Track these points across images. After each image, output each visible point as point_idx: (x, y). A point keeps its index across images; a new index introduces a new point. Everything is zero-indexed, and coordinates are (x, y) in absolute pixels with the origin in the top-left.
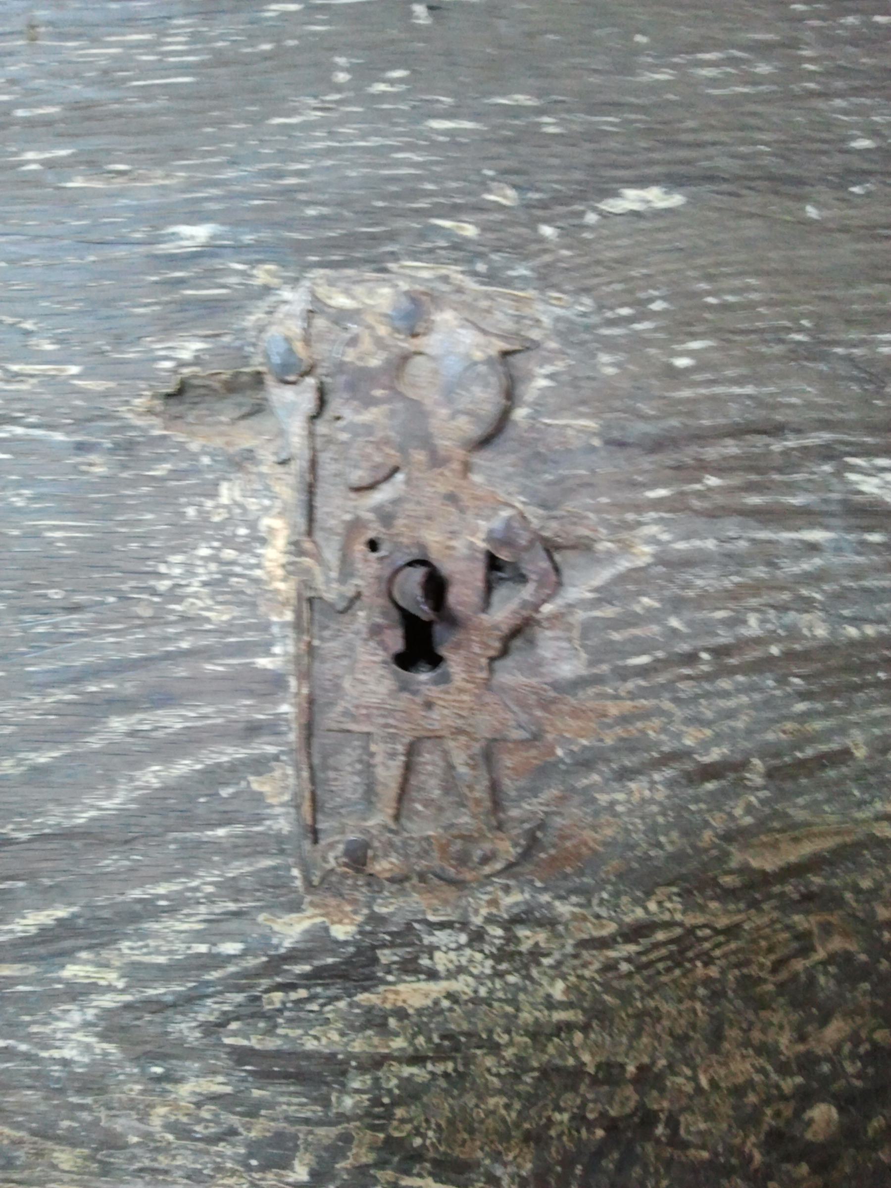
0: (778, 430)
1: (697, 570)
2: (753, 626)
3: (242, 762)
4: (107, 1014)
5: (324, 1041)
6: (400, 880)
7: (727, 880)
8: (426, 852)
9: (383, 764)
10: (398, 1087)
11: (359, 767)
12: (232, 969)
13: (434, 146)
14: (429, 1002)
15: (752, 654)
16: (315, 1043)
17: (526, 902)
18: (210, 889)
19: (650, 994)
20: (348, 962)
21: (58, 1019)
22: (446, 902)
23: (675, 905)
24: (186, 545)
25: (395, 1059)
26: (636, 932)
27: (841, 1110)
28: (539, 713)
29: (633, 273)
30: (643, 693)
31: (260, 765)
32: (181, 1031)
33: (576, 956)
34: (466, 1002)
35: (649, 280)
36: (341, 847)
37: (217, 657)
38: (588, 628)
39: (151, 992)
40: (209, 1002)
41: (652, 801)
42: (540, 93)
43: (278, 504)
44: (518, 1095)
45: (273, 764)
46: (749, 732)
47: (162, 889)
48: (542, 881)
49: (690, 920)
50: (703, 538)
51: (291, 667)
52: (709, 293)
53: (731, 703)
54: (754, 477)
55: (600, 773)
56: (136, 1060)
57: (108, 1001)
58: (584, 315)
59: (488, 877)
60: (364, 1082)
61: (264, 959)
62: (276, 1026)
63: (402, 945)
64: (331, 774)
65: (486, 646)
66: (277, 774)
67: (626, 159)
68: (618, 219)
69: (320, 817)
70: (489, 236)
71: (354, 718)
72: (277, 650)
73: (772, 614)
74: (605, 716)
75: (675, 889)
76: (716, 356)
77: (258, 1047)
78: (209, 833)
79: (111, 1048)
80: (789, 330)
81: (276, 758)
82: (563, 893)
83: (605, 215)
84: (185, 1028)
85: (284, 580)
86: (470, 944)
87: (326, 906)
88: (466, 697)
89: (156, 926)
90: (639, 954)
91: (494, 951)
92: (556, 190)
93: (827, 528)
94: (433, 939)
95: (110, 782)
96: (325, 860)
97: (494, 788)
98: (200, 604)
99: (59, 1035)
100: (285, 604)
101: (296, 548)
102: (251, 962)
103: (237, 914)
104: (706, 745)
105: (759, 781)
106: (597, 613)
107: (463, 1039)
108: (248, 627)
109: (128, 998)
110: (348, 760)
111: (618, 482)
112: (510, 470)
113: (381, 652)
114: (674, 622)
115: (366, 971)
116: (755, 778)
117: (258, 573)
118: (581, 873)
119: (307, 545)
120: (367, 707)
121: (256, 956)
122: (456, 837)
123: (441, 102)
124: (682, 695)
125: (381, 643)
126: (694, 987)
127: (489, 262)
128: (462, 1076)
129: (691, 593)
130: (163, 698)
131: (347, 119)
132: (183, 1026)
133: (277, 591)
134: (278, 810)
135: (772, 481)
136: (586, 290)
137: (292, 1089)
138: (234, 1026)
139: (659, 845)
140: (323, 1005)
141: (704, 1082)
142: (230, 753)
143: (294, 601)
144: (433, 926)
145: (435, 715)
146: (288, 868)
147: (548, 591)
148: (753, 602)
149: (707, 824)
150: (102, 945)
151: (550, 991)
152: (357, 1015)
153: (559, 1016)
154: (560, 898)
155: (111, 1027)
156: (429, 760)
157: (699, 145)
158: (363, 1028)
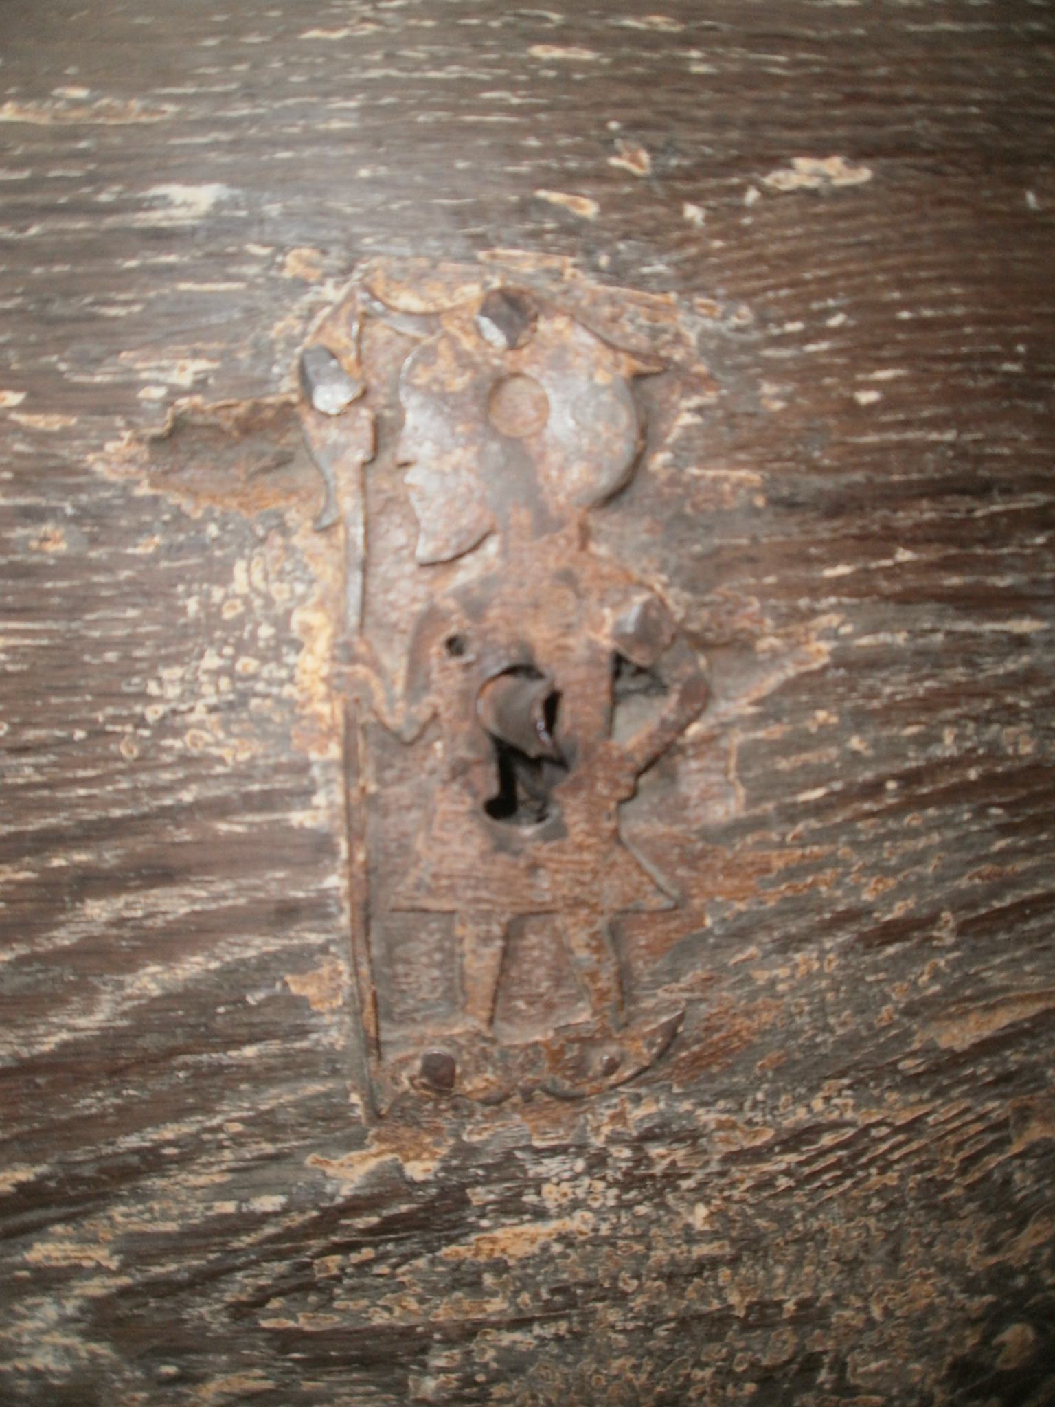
0: (983, 490)
1: (884, 674)
2: (948, 746)
3: (275, 956)
4: (97, 1305)
5: (397, 1311)
6: (496, 1102)
7: (906, 1065)
8: (533, 1063)
9: (474, 952)
10: (496, 1360)
11: (438, 957)
12: (270, 1230)
13: (535, 83)
14: (535, 1249)
15: (947, 781)
16: (386, 1315)
17: (661, 1113)
18: (238, 1127)
19: (813, 1213)
20: (429, 1207)
21: (23, 1317)
22: (557, 1122)
23: (848, 1099)
24: (188, 653)
27: (1040, 1330)
28: (682, 872)
29: (807, 276)
30: (816, 837)
31: (301, 960)
32: (201, 1318)
33: (722, 1174)
34: (583, 1244)
35: (826, 287)
36: (418, 1064)
38: (749, 754)
39: (156, 1270)
40: (239, 1276)
41: (820, 974)
42: (685, 15)
43: (317, 590)
44: (650, 1353)
45: (317, 957)
46: (940, 879)
47: (170, 1132)
48: (680, 1083)
49: (862, 1119)
51: (339, 823)
52: (903, 305)
53: (921, 843)
54: (953, 551)
55: (760, 944)
57: (95, 1287)
58: (739, 329)
60: (451, 1357)
61: (315, 1213)
62: (332, 1299)
65: (616, 784)
66: (325, 971)
68: (790, 198)
69: (384, 1025)
70: (616, 216)
71: (432, 892)
73: (971, 727)
74: (768, 871)
76: (907, 389)
77: (308, 1328)
78: (233, 1053)
79: (103, 1349)
80: (1000, 357)
81: (324, 949)
82: (707, 1098)
83: (766, 193)
84: (207, 1312)
85: (328, 698)
86: (588, 1171)
88: (587, 856)
90: (800, 1164)
91: (619, 1176)
93: (1036, 616)
94: (540, 1169)
95: (86, 991)
96: (396, 1081)
97: (624, 976)
98: (207, 737)
99: (26, 1339)
100: (330, 733)
101: (345, 653)
102: (297, 1219)
104: (887, 899)
105: (950, 940)
106: (760, 734)
107: (579, 1291)
108: (278, 769)
109: (125, 1281)
110: (423, 948)
111: (788, 556)
112: (645, 537)
114: (855, 743)
115: (453, 1217)
116: (945, 936)
117: (288, 690)
118: (730, 1070)
119: (361, 649)
120: (449, 877)
121: (302, 1211)
122: (572, 1041)
123: (547, 20)
124: (862, 838)
125: (467, 785)
126: (868, 1199)
127: (614, 254)
130: (162, 873)
131: (412, 37)
132: (204, 1310)
133: (318, 717)
134: (327, 1019)
136: (746, 296)
137: (355, 1376)
138: (275, 1304)
139: (827, 1028)
141: (876, 1312)
142: (257, 946)
143: (341, 730)
144: (540, 1153)
146: (346, 1094)
147: (697, 706)
148: (950, 713)
150: (86, 1214)
151: (690, 1220)
152: (440, 1274)
153: (702, 1250)
154: (703, 1104)
155: (102, 1319)
156: (534, 941)
157: (892, 101)
158: (453, 1287)
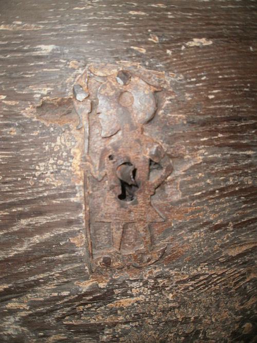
6: (121, 269)
8: (130, 259)
9: (115, 232)
13: (130, 20)
17: (161, 271)
18: (58, 275)
19: (198, 296)
20: (105, 294)
21: (6, 321)
22: (136, 273)
25: (120, 323)
26: (194, 278)
30: (199, 204)
31: (73, 234)
32: (49, 321)
33: (176, 286)
35: (201, 70)
36: (102, 259)
37: (57, 198)
38: (182, 184)
39: (38, 310)
40: (58, 311)
44: (158, 330)
46: (229, 214)
47: (41, 276)
50: (218, 154)
52: (220, 74)
53: (225, 206)
56: (34, 331)
57: (23, 314)
58: (180, 80)
59: (149, 265)
62: (81, 317)
63: (121, 288)
64: (97, 236)
66: (79, 237)
67: (194, 28)
68: (193, 48)
71: (105, 218)
72: (78, 195)
73: (237, 177)
74: (187, 212)
75: (206, 264)
79: (25, 329)
81: (79, 231)
83: (187, 47)
84: (50, 320)
85: (80, 170)
86: (143, 286)
87: (97, 277)
89: (39, 288)
92: (172, 38)
94: (131, 285)
96: (96, 264)
97: (152, 238)
99: (6, 326)
100: (80, 179)
101: (84, 159)
102: (72, 297)
103: (67, 282)
104: (216, 219)
105: (232, 229)
107: (141, 315)
108: (68, 187)
109: (31, 312)
111: (192, 136)
112: (157, 131)
113: (114, 195)
114: (208, 181)
115: (110, 297)
117: (70, 168)
125: (114, 191)
126: (211, 292)
128: (141, 326)
129: (213, 172)
130: (39, 213)
131: (100, 9)
134: (80, 249)
135: (237, 136)
136: (182, 72)
138: (67, 318)
140: (96, 309)
142: (63, 231)
145: (132, 215)
147: (170, 172)
148: (231, 174)
149: (216, 244)
150: (21, 296)
153: (171, 305)
154: (171, 269)
